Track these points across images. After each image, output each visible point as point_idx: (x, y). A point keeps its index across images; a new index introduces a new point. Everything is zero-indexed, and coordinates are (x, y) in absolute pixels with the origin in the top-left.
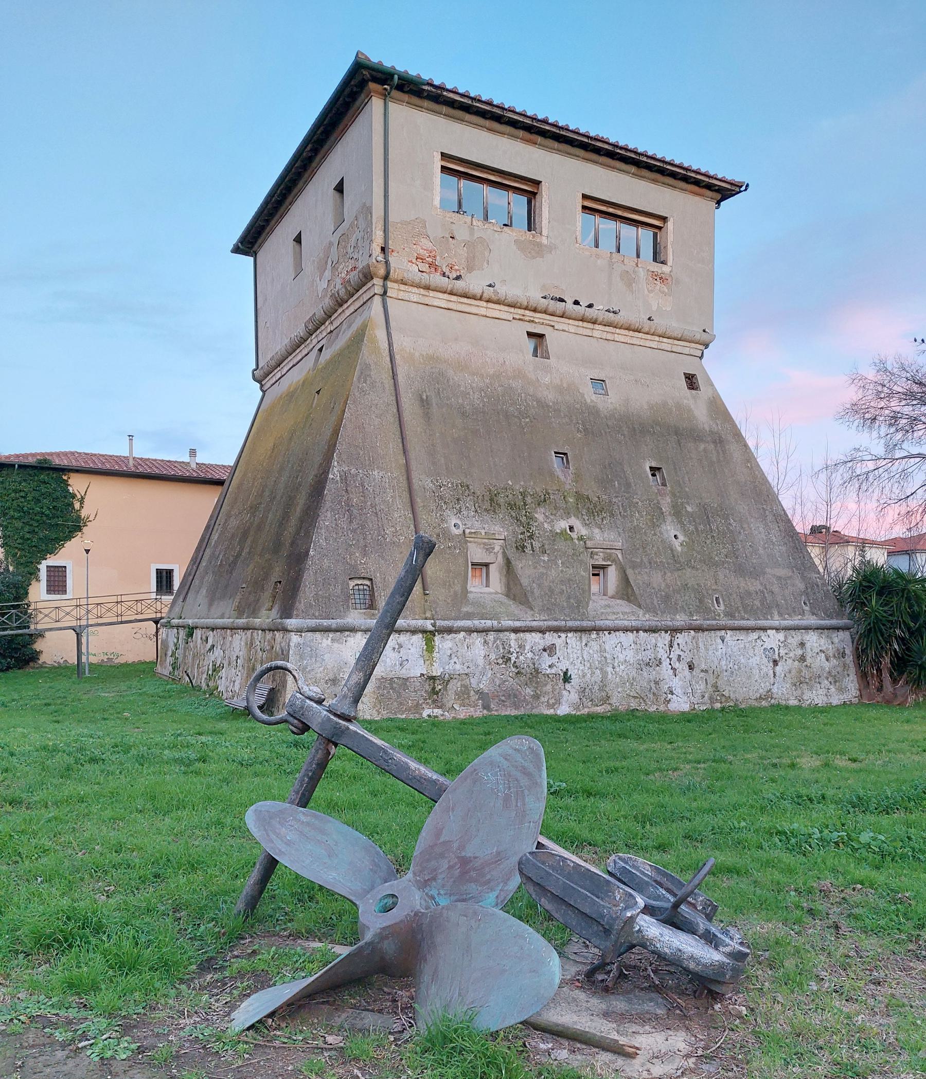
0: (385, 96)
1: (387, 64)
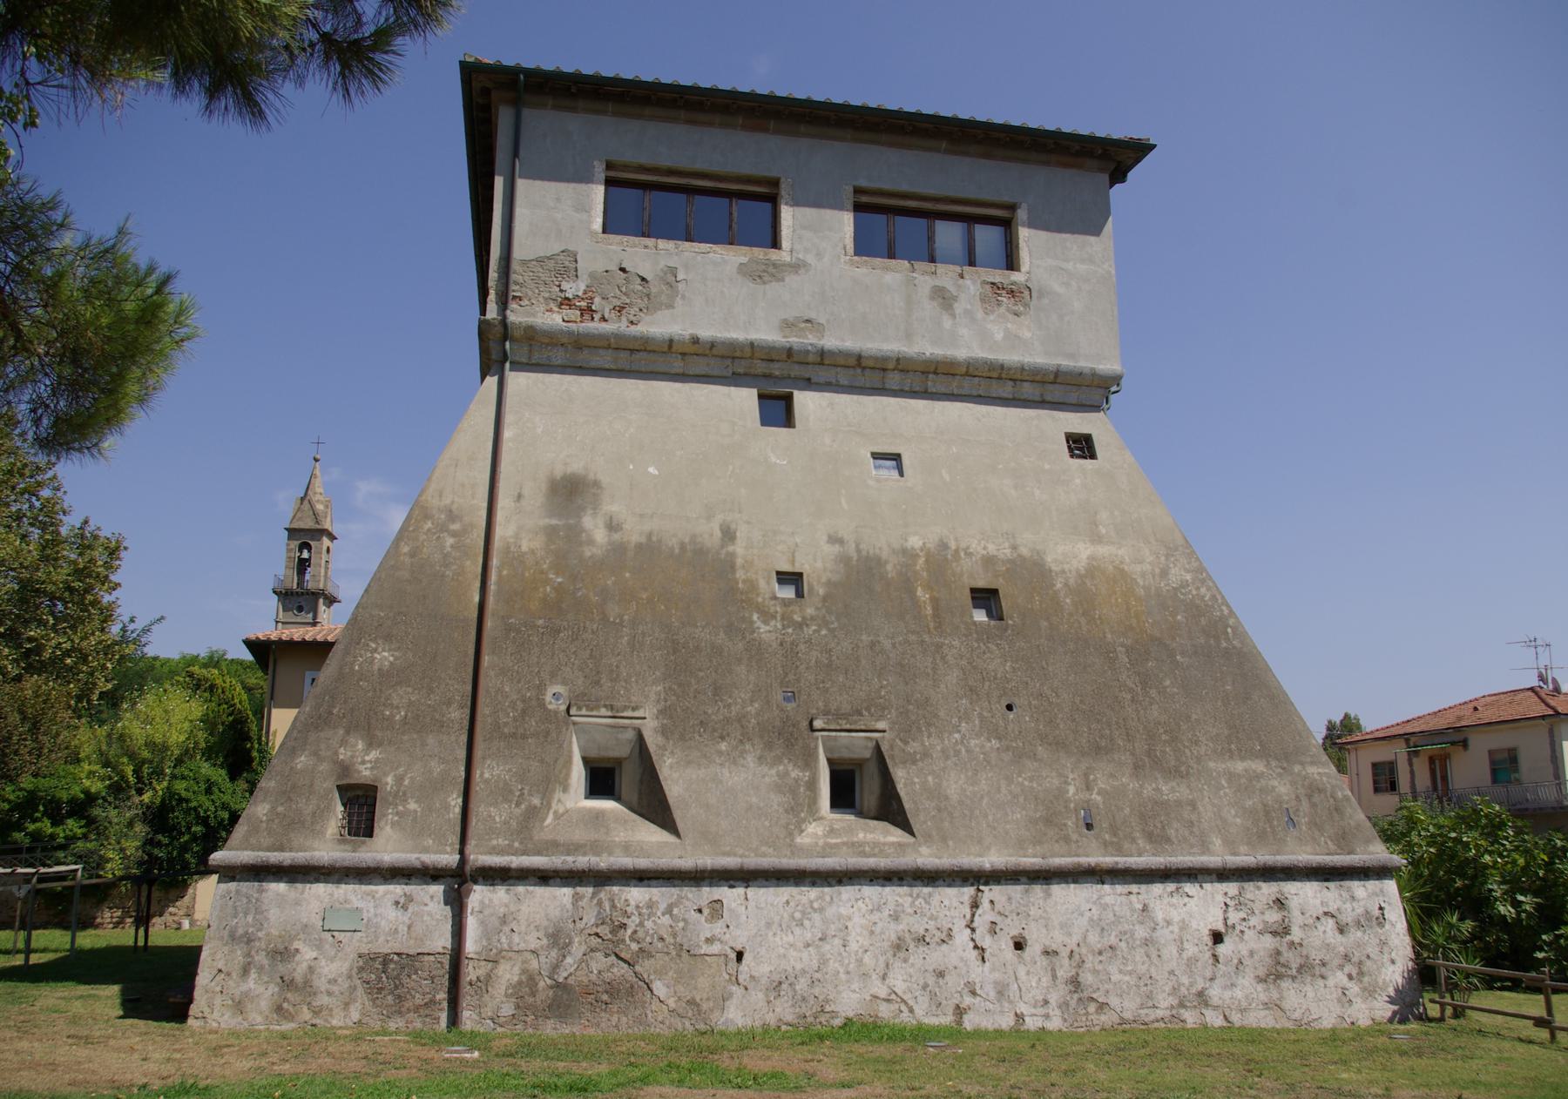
0: (517, 104)
1: (509, 61)
